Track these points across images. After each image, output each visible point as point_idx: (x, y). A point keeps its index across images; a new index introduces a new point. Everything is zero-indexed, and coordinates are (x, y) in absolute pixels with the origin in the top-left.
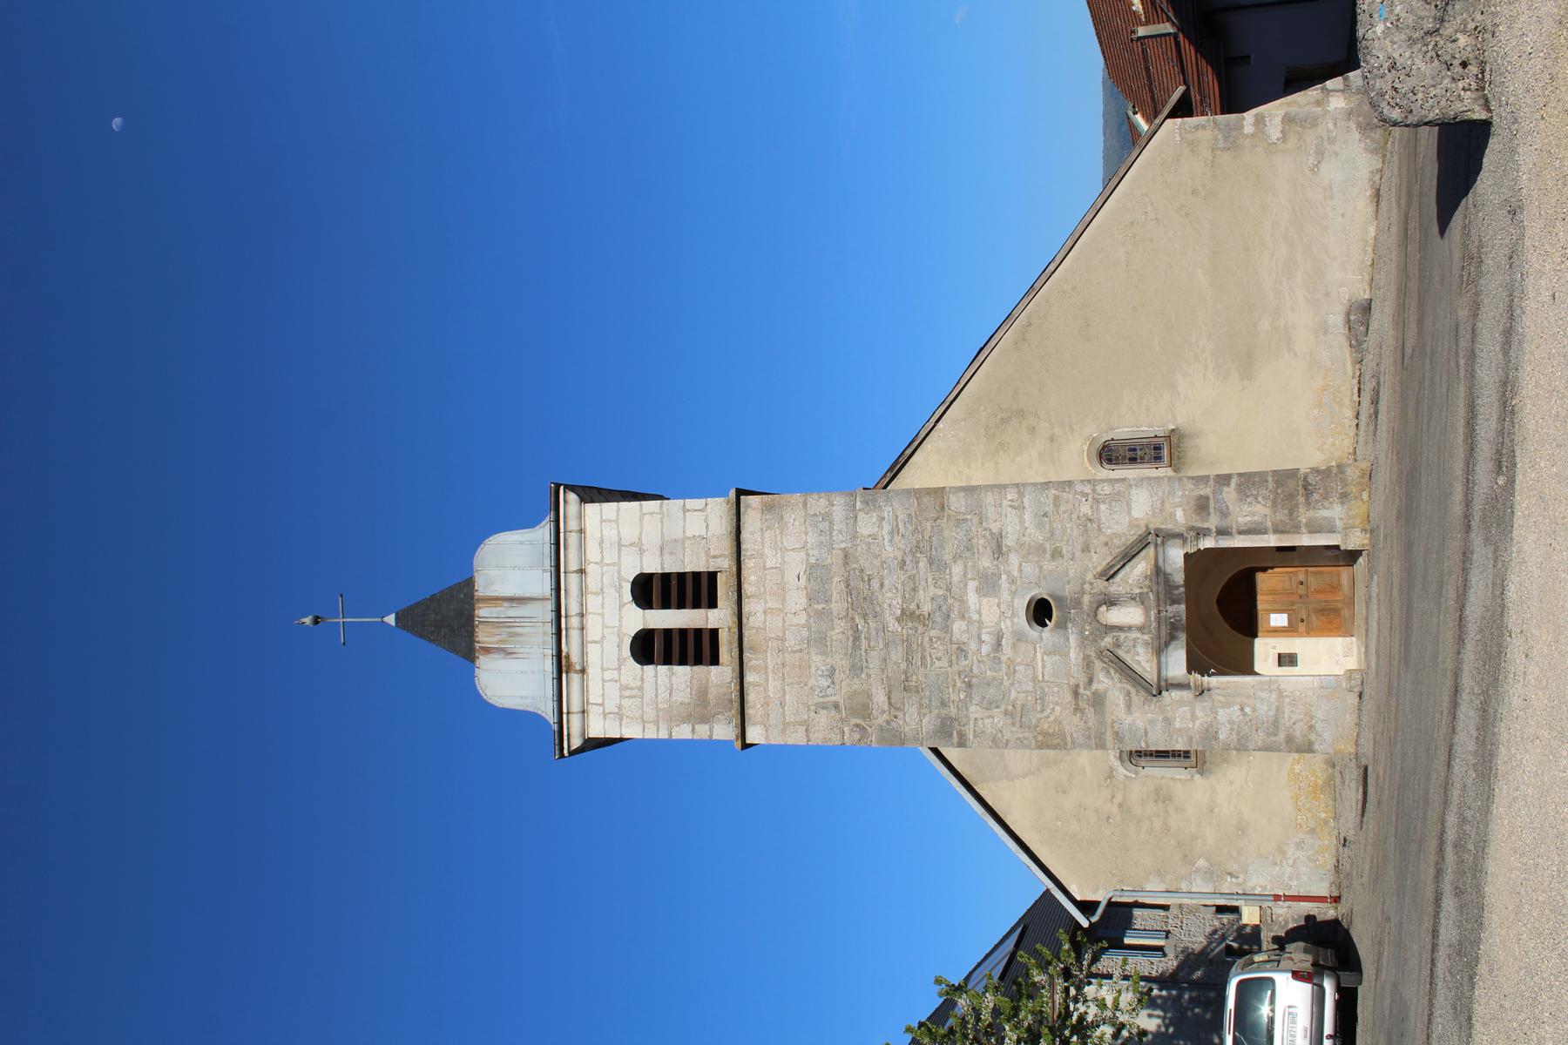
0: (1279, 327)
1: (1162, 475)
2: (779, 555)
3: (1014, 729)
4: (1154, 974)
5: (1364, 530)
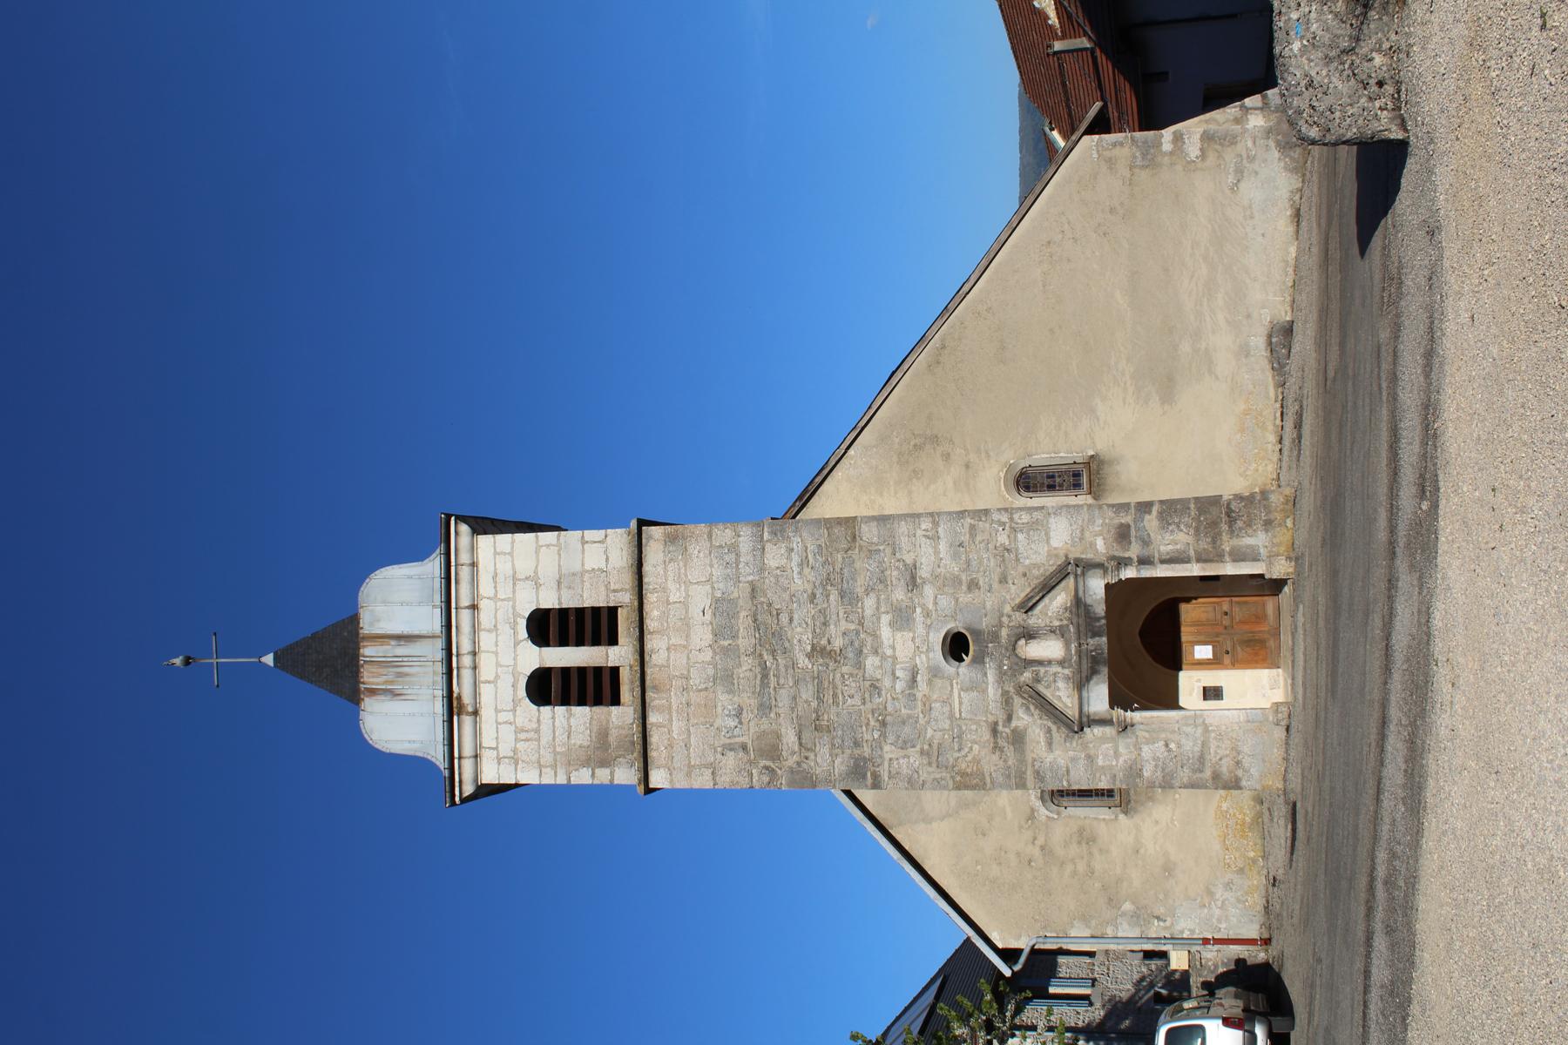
1: (1081, 503)
2: (683, 588)
3: (930, 769)
4: (1080, 1024)
5: (1289, 558)
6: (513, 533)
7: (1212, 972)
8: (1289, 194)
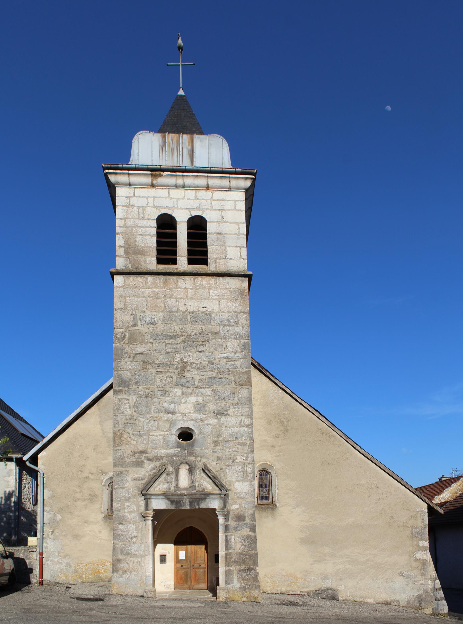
2: (217, 297)
3: (123, 420)
4: (23, 500)
5: (227, 598)
7: (26, 557)
8: (397, 600)
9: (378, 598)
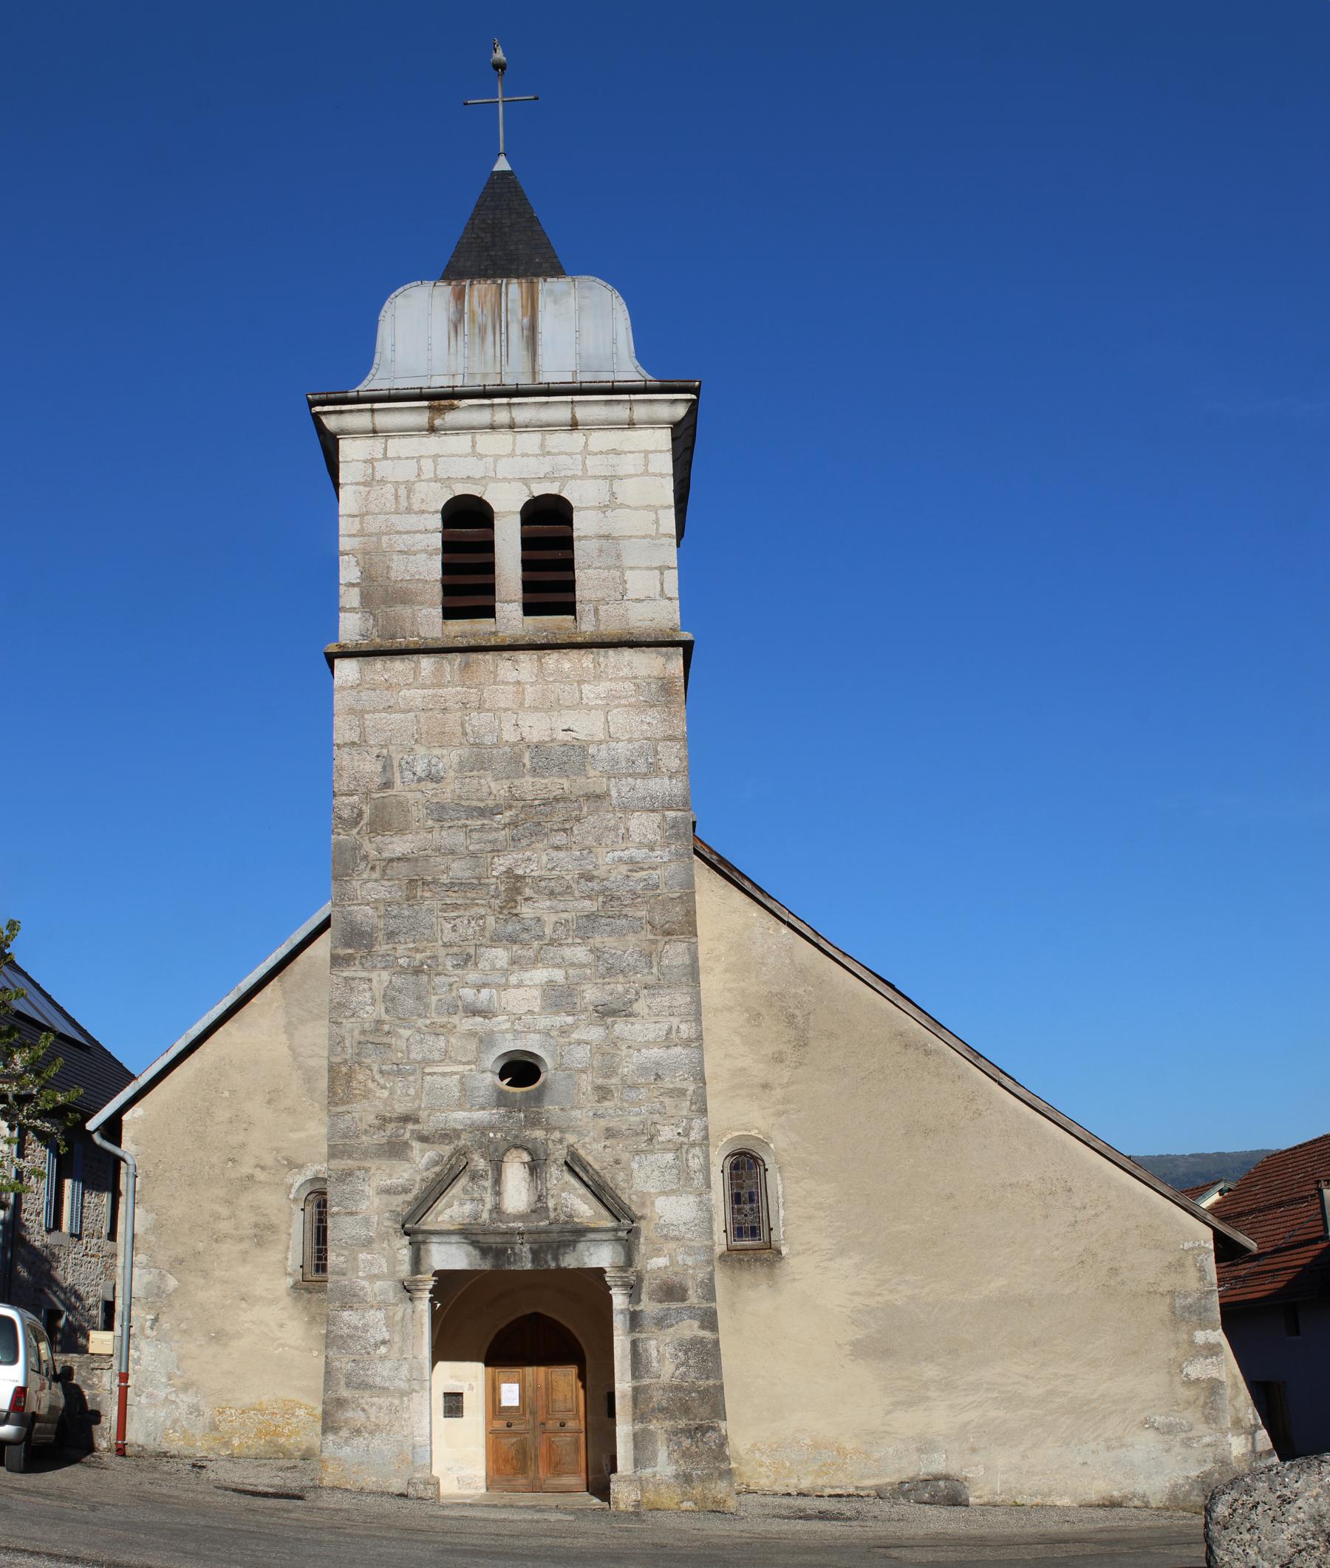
0: (928, 1390)
1: (716, 1238)
2: (600, 702)
3: (356, 1033)
4: (25, 1216)
5: (638, 1504)
6: (674, 475)
7: (84, 1382)
8: (1141, 1492)
9: (1086, 1493)
